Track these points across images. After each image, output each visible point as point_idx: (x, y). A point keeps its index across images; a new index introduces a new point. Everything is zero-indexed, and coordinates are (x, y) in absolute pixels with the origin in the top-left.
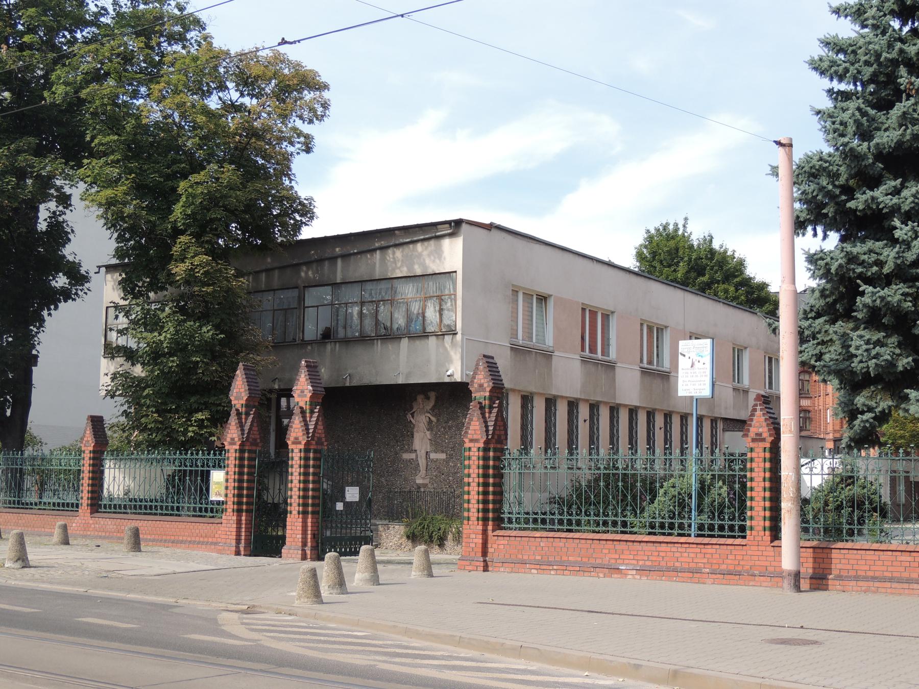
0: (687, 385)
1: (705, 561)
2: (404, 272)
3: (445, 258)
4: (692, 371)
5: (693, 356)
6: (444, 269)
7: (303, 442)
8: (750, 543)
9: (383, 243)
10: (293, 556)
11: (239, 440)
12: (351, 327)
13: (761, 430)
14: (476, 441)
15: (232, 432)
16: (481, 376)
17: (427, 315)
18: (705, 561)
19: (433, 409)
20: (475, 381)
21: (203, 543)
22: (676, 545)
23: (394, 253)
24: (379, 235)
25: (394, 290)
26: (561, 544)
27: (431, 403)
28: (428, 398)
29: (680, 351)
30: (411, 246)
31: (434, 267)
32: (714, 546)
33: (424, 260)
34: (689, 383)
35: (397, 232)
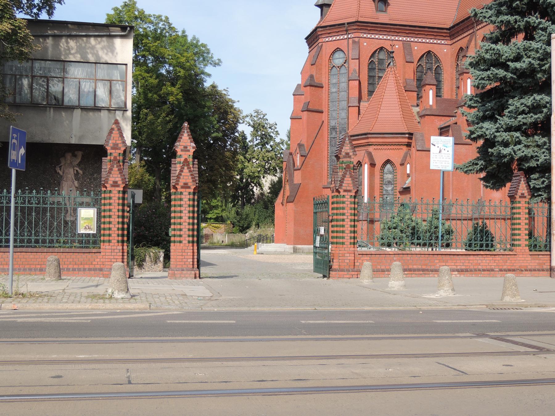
1: (495, 264)
2: (78, 58)
3: (117, 53)
4: (440, 155)
6: (116, 61)
7: (193, 187)
8: (519, 253)
9: (56, 32)
10: (187, 276)
11: (123, 183)
12: (20, 94)
13: (524, 192)
14: (349, 191)
15: (114, 176)
17: (97, 93)
18: (495, 264)
19: (79, 165)
20: (343, 150)
21: (79, 270)
22: (479, 256)
23: (67, 43)
24: (51, 24)
25: (64, 70)
26: (408, 258)
27: (79, 160)
28: (75, 156)
29: (432, 142)
30: (85, 39)
31: (105, 57)
32: (500, 256)
33: (97, 51)
34: (438, 162)
35: (69, 25)
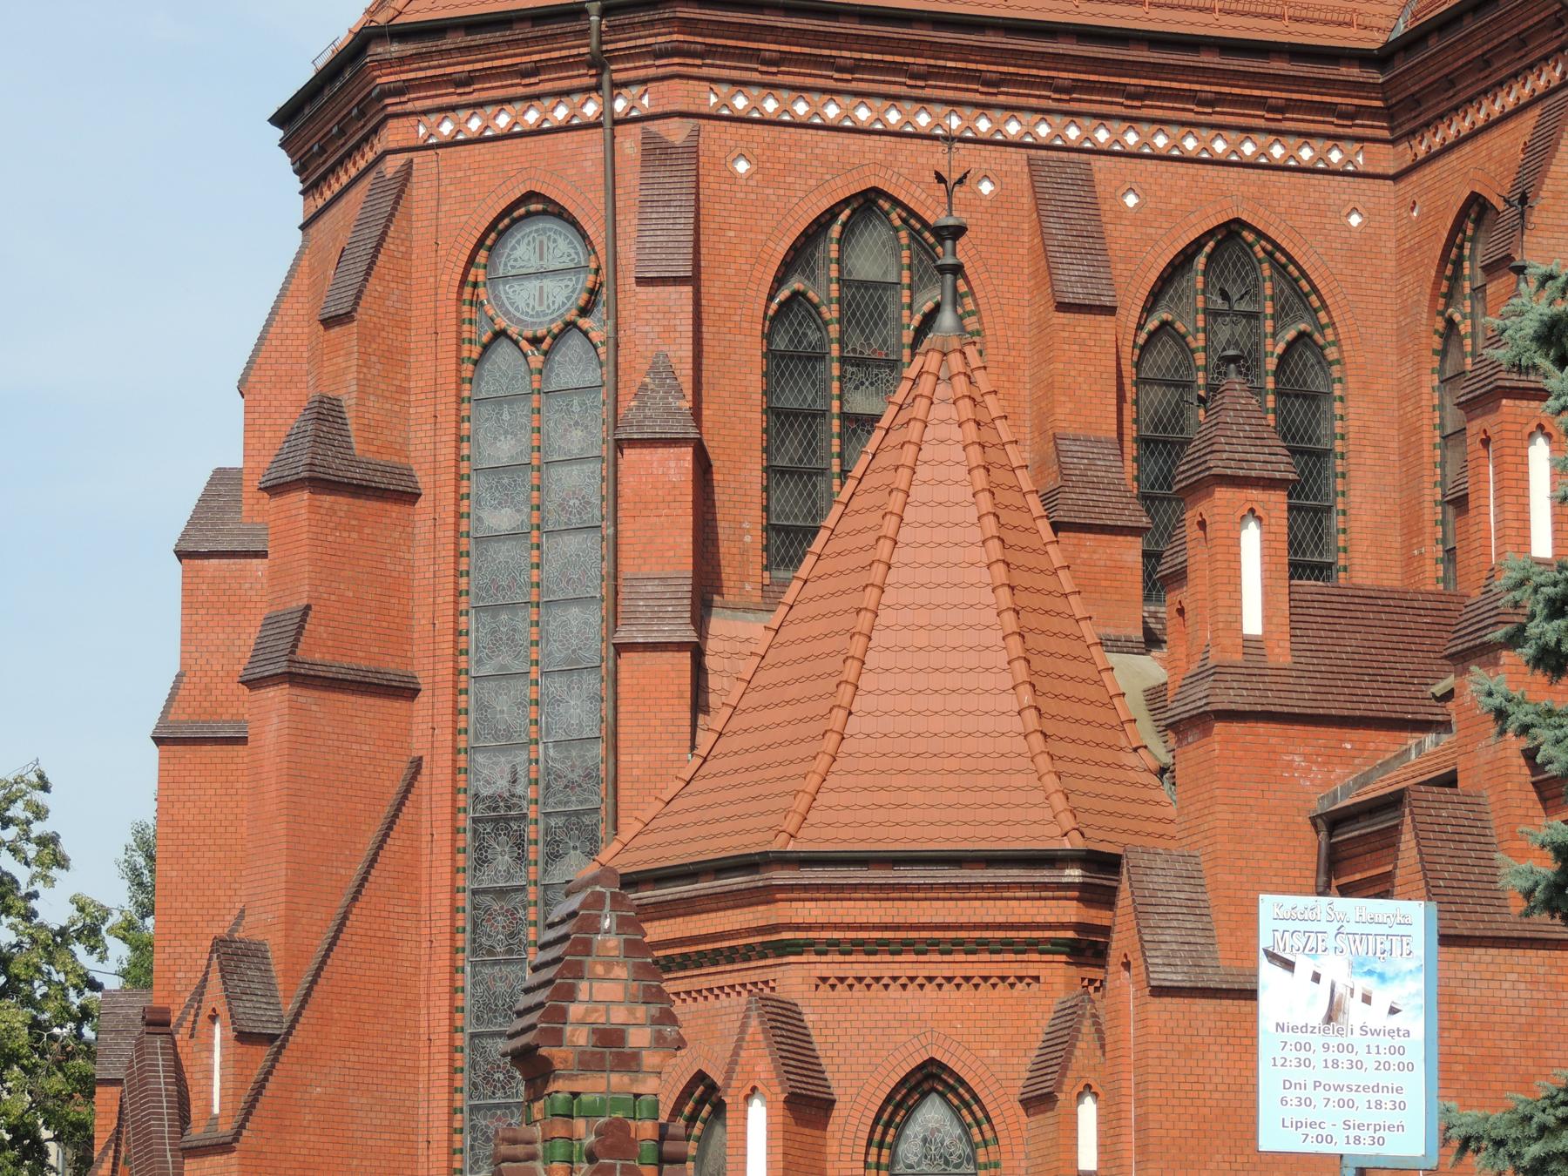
0: (1308, 1102)
4: (1334, 1041)
5: (1336, 969)
16: (609, 990)
29: (1265, 941)
34: (1318, 1096)
